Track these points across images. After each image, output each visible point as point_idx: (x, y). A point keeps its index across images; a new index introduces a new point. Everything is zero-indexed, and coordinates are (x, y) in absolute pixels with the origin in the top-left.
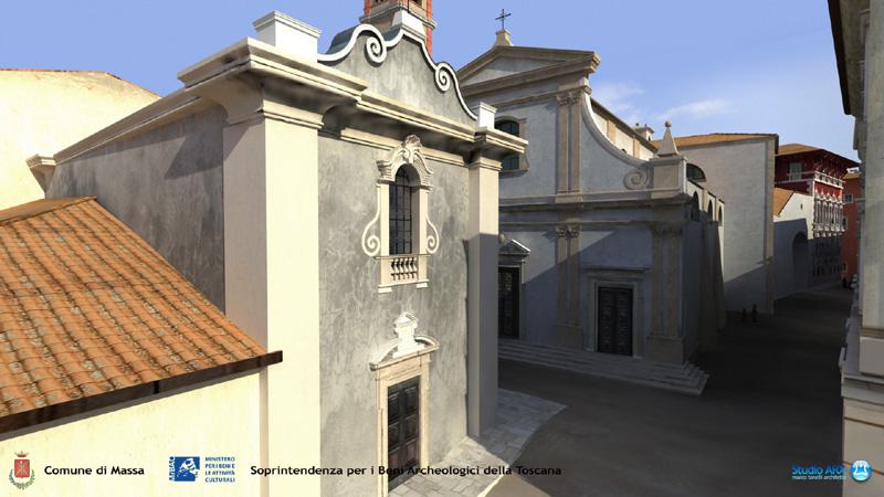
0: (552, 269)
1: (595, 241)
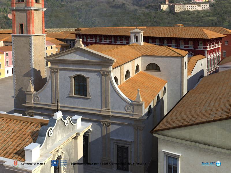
0: (100, 138)
1: (115, 129)
